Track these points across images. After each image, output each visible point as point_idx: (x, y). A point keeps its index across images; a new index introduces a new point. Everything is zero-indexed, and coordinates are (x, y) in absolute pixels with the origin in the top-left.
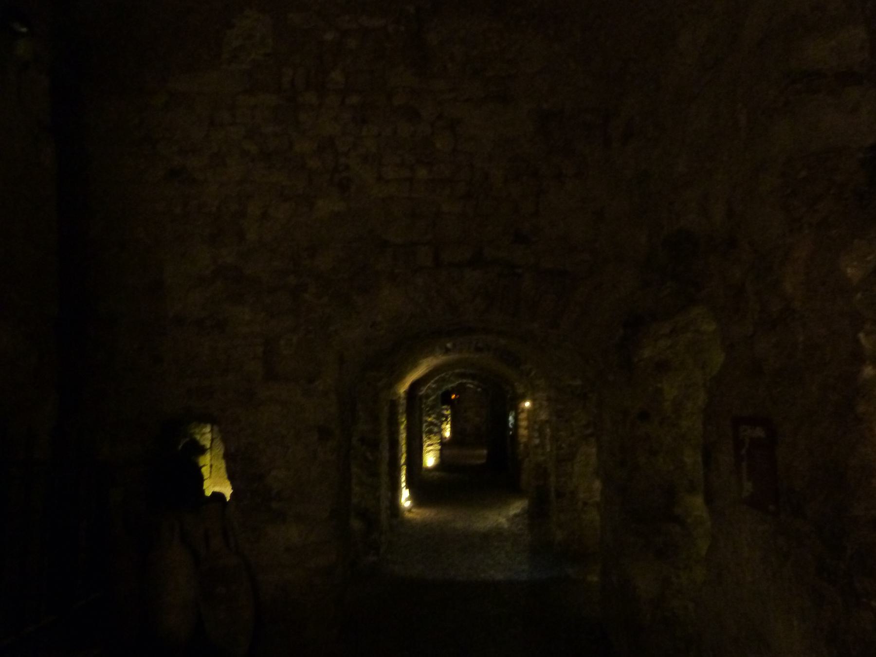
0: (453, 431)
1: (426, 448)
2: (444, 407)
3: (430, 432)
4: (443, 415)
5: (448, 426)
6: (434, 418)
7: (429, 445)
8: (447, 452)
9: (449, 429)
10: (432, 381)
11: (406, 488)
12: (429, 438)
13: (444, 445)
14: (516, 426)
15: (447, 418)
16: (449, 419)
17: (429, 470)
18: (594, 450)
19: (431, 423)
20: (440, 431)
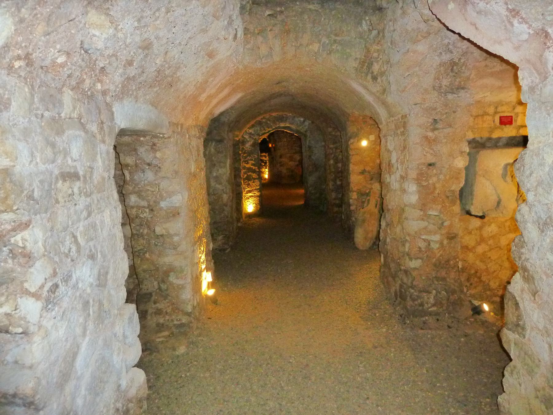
0: (269, 175)
1: (245, 195)
2: (264, 154)
3: (248, 178)
4: (262, 161)
5: (267, 170)
6: (253, 165)
7: (250, 192)
8: (265, 192)
9: (267, 173)
10: (248, 126)
11: (207, 271)
12: (249, 185)
13: (264, 186)
14: (109, 140)
15: (266, 163)
16: (268, 164)
17: (250, 216)
18: (267, 158)
19: (249, 170)
20: (260, 173)
